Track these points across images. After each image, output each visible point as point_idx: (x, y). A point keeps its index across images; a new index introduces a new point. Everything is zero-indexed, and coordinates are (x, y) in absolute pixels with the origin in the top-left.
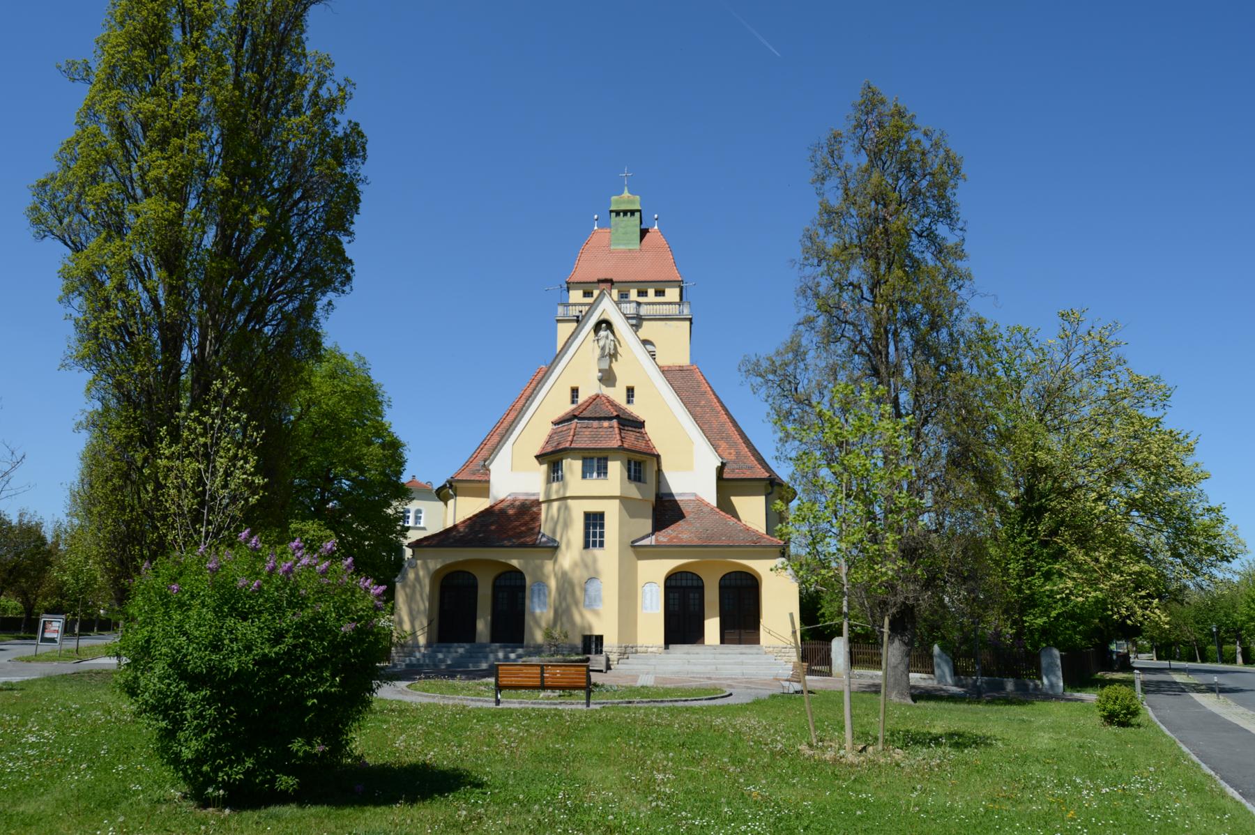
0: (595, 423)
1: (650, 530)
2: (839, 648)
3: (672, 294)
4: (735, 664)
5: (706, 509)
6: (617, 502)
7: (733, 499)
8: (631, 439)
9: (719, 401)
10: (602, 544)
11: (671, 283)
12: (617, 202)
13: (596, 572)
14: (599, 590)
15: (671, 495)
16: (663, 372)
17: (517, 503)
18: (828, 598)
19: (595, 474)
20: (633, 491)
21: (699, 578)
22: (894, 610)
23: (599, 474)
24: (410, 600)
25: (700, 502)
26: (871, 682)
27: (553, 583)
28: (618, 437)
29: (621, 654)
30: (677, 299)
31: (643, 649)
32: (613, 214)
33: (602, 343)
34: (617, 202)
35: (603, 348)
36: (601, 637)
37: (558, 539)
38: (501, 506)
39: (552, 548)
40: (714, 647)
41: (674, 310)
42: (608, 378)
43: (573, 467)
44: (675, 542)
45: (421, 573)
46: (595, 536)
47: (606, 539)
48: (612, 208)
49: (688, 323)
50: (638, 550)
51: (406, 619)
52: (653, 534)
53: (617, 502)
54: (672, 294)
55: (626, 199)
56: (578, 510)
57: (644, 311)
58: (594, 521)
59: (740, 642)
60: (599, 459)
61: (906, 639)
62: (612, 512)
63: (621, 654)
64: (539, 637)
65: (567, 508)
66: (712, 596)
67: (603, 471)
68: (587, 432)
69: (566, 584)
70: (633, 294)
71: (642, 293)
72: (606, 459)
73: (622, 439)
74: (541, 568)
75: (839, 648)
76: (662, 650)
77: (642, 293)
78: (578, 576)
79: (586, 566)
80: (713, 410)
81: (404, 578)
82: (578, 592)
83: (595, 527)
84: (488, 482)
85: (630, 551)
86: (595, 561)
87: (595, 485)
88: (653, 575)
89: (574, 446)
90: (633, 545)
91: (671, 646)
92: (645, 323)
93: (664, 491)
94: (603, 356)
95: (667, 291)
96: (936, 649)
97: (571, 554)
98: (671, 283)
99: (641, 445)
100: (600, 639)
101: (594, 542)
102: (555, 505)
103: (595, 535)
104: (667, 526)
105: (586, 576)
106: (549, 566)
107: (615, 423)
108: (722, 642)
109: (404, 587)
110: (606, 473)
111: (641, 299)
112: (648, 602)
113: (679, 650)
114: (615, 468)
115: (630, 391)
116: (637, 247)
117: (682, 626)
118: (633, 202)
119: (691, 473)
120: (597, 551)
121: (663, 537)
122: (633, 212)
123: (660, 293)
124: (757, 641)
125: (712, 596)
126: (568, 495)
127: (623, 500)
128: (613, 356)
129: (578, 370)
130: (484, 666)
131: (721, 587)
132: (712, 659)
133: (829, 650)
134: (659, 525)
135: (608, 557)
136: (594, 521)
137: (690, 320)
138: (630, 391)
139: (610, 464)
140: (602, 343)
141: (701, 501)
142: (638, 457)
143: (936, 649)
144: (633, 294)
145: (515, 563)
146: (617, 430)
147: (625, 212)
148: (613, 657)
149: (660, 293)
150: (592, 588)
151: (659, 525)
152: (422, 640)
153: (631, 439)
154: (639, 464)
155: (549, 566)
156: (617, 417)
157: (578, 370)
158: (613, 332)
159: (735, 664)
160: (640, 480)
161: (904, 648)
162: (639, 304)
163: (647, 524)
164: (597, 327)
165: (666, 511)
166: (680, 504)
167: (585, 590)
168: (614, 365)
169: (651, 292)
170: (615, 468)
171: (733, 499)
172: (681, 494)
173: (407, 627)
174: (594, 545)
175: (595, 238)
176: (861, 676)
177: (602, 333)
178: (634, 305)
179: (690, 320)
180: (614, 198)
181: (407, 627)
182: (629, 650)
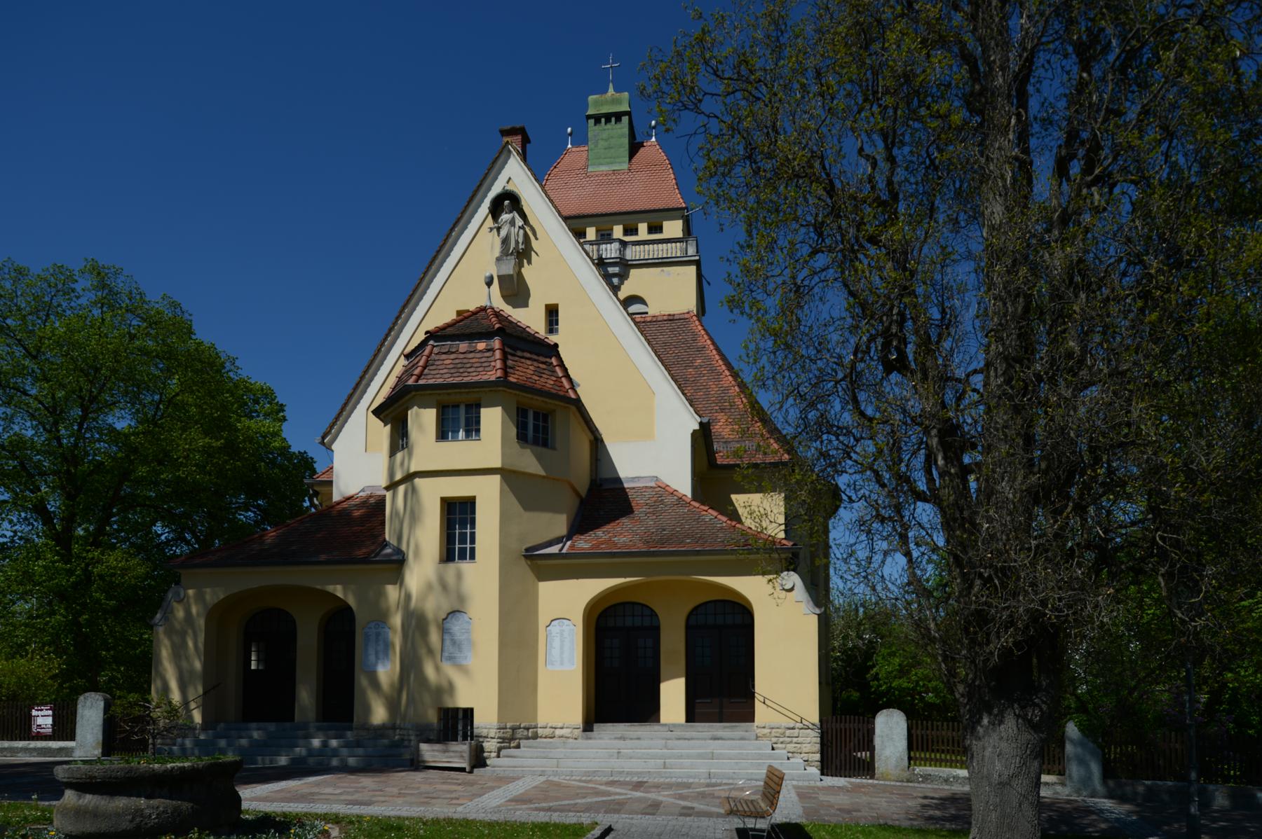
0: (463, 346)
2: (890, 730)
3: (673, 228)
4: (700, 756)
5: (669, 500)
6: (497, 478)
7: (733, 497)
8: (525, 371)
9: (717, 349)
10: (473, 557)
11: (671, 213)
12: (596, 103)
13: (461, 598)
14: (468, 631)
15: (618, 480)
16: (566, 219)
17: (372, 501)
18: (884, 651)
19: (461, 434)
20: (529, 462)
21: (653, 614)
22: (1007, 640)
23: (468, 435)
24: (179, 653)
25: (662, 492)
26: (947, 790)
27: (397, 620)
28: (499, 364)
29: (503, 740)
30: (680, 235)
31: (548, 732)
32: (592, 122)
33: (503, 233)
34: (596, 104)
35: (505, 241)
36: (472, 710)
37: (404, 548)
38: (345, 505)
39: (397, 564)
40: (671, 728)
41: (674, 250)
42: (516, 291)
43: (423, 420)
44: (604, 548)
45: (194, 610)
46: (463, 541)
47: (478, 546)
48: (591, 112)
49: (693, 269)
50: (539, 563)
51: (173, 685)
53: (497, 478)
54: (673, 228)
55: (614, 99)
56: (432, 493)
57: (631, 253)
58: (458, 513)
59: (720, 718)
60: (469, 407)
61: (1035, 714)
62: (488, 496)
63: (503, 740)
65: (414, 490)
66: (673, 641)
67: (473, 428)
68: (448, 360)
69: (416, 623)
70: (618, 231)
71: (630, 230)
72: (479, 406)
73: (505, 368)
74: (382, 594)
75: (890, 730)
76: (578, 732)
77: (630, 230)
78: (433, 606)
79: (444, 586)
80: (713, 370)
81: (166, 618)
82: (434, 637)
83: (463, 526)
85: (524, 568)
86: (459, 576)
87: (459, 452)
88: (566, 603)
89: (421, 382)
90: (531, 555)
91: (596, 726)
92: (633, 272)
93: (605, 474)
94: (505, 252)
95: (666, 224)
96: (1072, 730)
97: (422, 571)
98: (671, 213)
99: (548, 383)
100: (469, 713)
104: (598, 526)
105: (446, 608)
106: (392, 592)
107: (496, 343)
108: (688, 720)
109: (170, 632)
110: (478, 431)
112: (555, 652)
113: (610, 735)
114: (492, 418)
115: (552, 313)
116: (626, 166)
117: (618, 692)
118: (618, 102)
119: (651, 440)
120: (466, 566)
121: (583, 543)
122: (618, 116)
123: (655, 228)
124: (750, 717)
125: (673, 641)
126: (412, 470)
127: (508, 475)
128: (524, 253)
129: (463, 281)
130: (283, 761)
131: (689, 628)
132: (672, 747)
133: (871, 732)
134: (580, 526)
135: (482, 577)
136: (458, 513)
137: (698, 264)
138: (552, 313)
139: (485, 412)
140: (503, 233)
141: (665, 488)
142: (538, 402)
143: (1072, 730)
144: (618, 231)
145: (338, 591)
146: (498, 354)
147: (608, 117)
148: (490, 746)
149: (655, 228)
150: (456, 627)
151: (580, 526)
152: (197, 717)
153: (525, 371)
154: (544, 418)
155: (392, 592)
156: (501, 332)
157: (463, 281)
158: (523, 216)
159: (700, 756)
160: (545, 444)
161: (1029, 736)
162: (624, 244)
163: (558, 524)
164: (496, 209)
165: (603, 499)
166: (630, 493)
167: (444, 631)
168: (527, 271)
169: (643, 228)
170: (492, 418)
171: (733, 497)
172: (633, 479)
173: (176, 697)
174: (462, 557)
175: (567, 160)
176: (926, 778)
177: (505, 217)
178: (616, 245)
180: (591, 98)
181: (176, 697)
182: (520, 733)
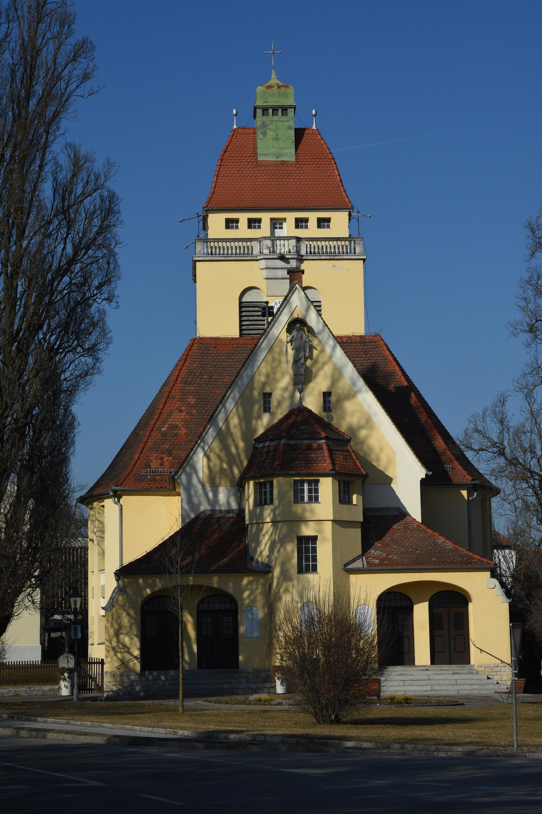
1: (360, 552)
10: (315, 569)
11: (291, 107)
40: (425, 669)
52: (362, 555)
60: (310, 484)
64: (32, 689)
84: (316, 556)
101: (307, 566)
102: (255, 526)
103: (307, 560)
108: (433, 662)
111: (301, 233)
120: (311, 577)
122: (285, 109)
124: (467, 661)
137: (364, 260)
147: (275, 110)
162: (299, 240)
179: (364, 260)
